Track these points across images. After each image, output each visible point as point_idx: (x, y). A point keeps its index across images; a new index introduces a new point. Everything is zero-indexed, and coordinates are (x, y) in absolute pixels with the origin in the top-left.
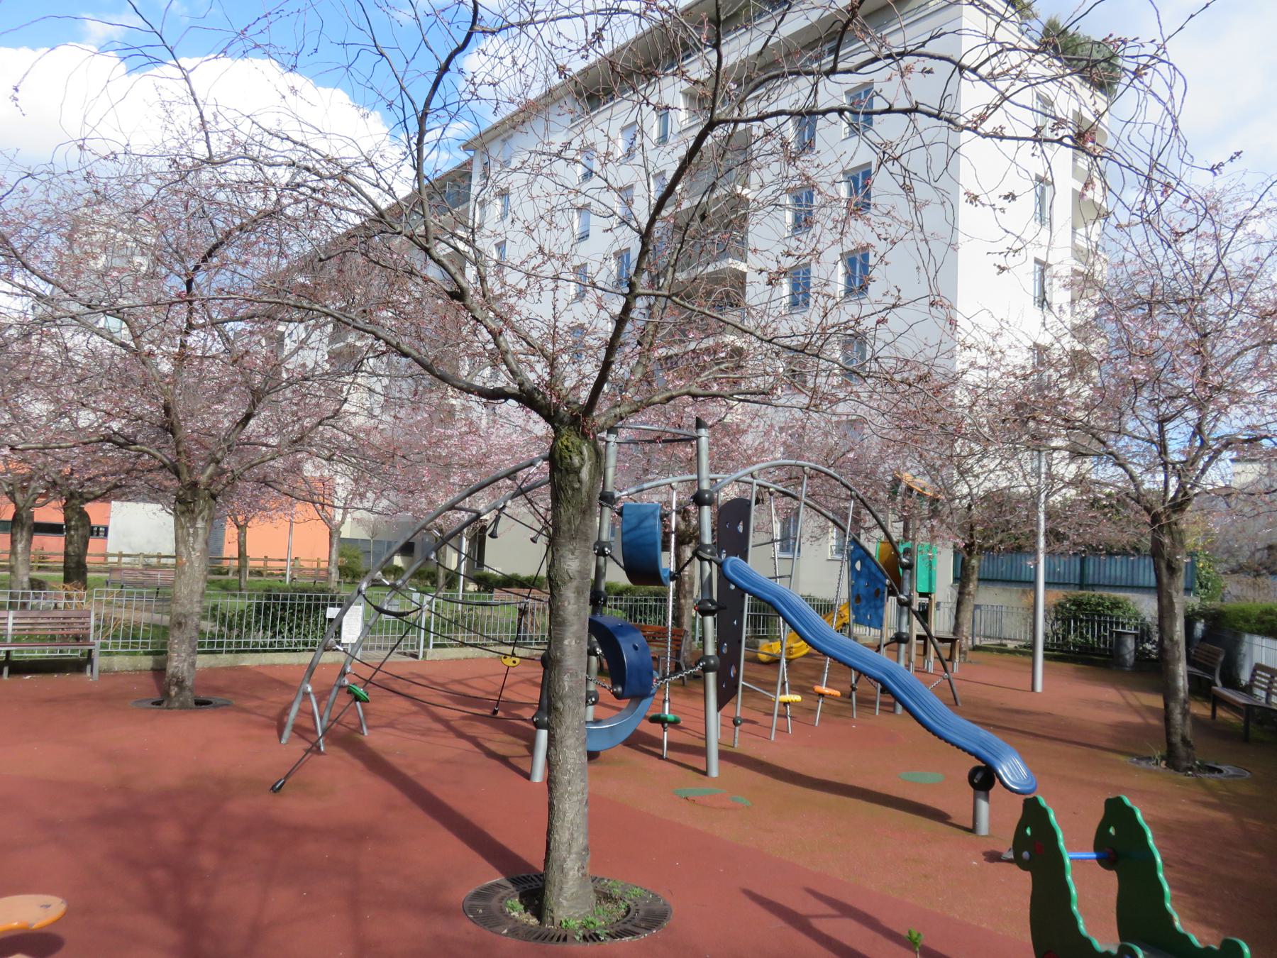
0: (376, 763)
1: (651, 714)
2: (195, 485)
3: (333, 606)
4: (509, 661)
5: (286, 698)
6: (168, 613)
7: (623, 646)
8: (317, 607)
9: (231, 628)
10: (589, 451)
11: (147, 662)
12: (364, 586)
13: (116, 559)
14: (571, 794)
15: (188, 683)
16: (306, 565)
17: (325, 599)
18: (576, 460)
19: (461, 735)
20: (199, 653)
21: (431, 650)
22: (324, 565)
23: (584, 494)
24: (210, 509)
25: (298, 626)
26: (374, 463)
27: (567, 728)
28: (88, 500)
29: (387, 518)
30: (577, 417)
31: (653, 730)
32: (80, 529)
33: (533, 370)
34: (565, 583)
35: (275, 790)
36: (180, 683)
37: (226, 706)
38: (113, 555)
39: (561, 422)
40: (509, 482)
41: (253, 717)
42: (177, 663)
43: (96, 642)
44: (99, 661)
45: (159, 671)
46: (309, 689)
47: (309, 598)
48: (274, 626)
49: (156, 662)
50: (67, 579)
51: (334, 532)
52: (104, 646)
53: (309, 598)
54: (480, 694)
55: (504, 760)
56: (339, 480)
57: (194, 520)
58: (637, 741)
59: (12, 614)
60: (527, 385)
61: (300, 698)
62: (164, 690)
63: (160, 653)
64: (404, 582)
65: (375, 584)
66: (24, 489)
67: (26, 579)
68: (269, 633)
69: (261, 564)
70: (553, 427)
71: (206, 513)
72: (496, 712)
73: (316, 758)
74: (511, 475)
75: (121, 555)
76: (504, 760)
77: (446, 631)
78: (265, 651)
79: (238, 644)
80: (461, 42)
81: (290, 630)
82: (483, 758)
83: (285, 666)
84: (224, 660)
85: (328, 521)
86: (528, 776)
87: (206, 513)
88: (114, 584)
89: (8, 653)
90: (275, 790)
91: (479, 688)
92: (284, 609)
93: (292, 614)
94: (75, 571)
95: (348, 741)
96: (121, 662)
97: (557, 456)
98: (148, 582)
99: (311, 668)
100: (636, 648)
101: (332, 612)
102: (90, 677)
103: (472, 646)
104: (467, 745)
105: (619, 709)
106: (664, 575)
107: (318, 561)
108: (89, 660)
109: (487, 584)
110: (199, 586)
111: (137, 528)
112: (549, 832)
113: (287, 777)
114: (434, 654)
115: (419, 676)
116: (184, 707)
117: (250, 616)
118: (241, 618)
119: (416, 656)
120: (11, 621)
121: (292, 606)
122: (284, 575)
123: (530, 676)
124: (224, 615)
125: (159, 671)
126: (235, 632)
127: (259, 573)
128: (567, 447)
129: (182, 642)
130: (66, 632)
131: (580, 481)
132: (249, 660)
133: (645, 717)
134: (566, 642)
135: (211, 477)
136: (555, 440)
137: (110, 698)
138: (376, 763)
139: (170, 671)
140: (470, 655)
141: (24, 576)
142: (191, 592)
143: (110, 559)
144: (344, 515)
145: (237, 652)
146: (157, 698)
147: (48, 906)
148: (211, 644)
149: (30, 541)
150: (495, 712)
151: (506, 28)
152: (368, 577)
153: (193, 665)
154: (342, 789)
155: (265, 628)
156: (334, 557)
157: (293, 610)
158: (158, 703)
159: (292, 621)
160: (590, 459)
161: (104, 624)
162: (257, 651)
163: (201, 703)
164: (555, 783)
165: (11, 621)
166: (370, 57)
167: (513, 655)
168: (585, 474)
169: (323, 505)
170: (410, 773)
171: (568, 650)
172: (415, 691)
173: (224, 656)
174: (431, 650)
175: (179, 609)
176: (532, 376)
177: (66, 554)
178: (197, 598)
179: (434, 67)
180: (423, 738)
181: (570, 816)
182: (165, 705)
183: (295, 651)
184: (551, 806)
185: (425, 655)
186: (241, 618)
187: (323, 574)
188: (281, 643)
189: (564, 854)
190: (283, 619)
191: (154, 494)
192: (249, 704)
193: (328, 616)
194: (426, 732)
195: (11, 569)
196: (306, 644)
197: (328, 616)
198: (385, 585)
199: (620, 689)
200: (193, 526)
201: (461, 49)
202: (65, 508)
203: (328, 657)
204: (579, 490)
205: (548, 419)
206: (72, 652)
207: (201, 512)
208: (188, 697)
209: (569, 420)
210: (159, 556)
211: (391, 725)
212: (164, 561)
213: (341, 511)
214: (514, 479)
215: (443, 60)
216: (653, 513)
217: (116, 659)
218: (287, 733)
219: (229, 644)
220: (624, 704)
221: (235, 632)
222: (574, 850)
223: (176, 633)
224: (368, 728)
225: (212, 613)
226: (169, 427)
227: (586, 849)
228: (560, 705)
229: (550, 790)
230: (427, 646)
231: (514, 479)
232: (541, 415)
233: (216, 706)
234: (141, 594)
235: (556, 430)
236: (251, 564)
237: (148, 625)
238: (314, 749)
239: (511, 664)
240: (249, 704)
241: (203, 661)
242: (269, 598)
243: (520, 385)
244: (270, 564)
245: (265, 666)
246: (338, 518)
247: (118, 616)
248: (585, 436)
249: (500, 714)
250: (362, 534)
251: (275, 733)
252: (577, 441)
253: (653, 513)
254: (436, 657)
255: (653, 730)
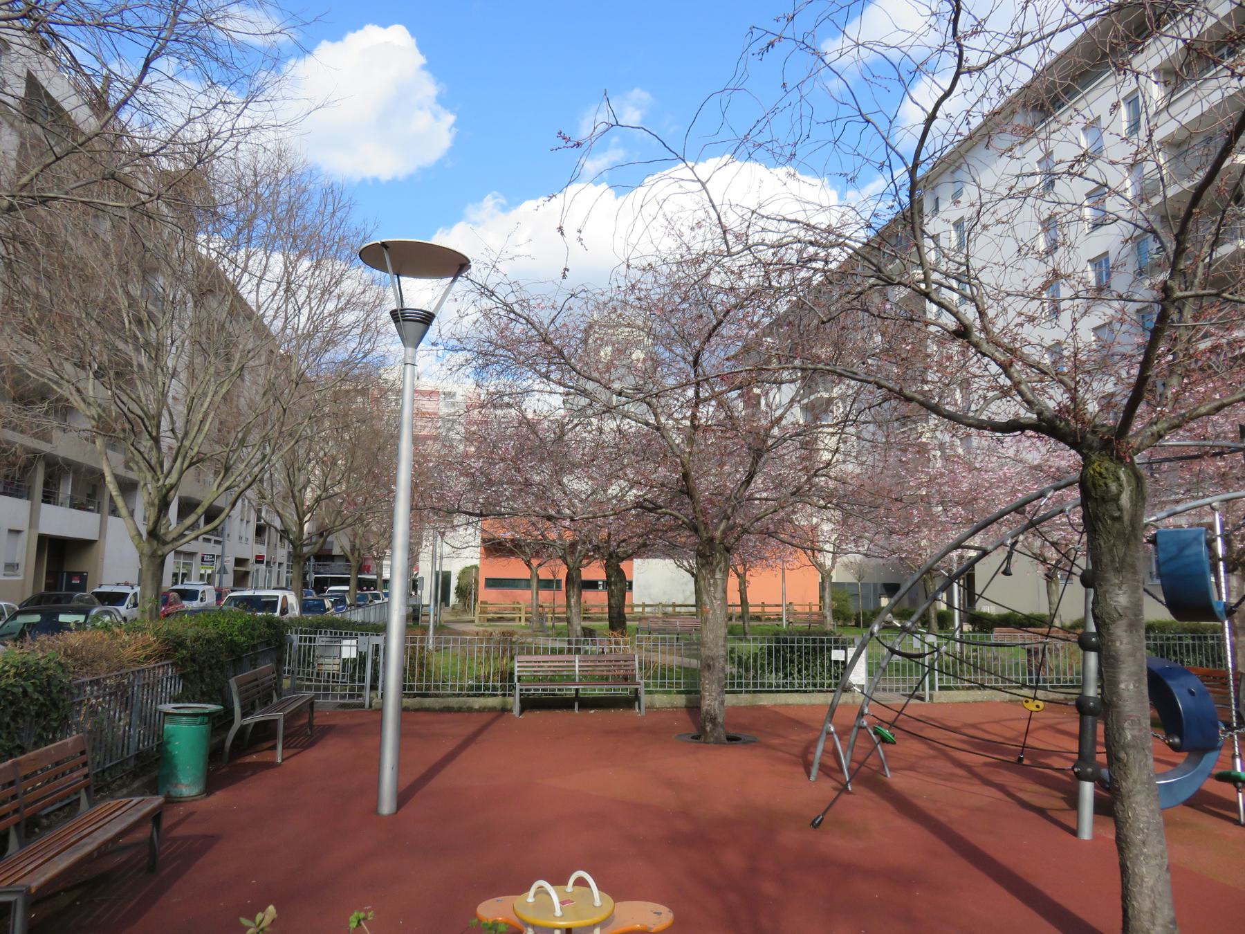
0: (903, 805)
1: (1216, 771)
2: (712, 539)
3: (837, 648)
4: (1031, 706)
5: (811, 736)
6: (697, 657)
7: (1175, 690)
8: (822, 649)
9: (747, 670)
10: (1128, 476)
11: (681, 700)
12: (876, 628)
13: (640, 609)
14: (1147, 857)
15: (720, 720)
16: (799, 609)
17: (829, 641)
18: (1113, 487)
19: (987, 782)
20: (727, 692)
21: (937, 692)
22: (815, 609)
23: (1126, 518)
24: (726, 561)
25: (807, 668)
26: (854, 505)
27: (1135, 782)
28: (623, 559)
29: (881, 561)
30: (1109, 441)
31: (1224, 790)
32: (619, 584)
33: (1051, 398)
34: (1114, 621)
35: (815, 825)
36: (713, 720)
37: (752, 743)
38: (638, 606)
39: (1090, 448)
40: (1019, 517)
41: (780, 754)
42: (710, 701)
43: (641, 681)
44: (645, 699)
45: (693, 708)
46: (832, 729)
47: (814, 641)
48: (785, 668)
49: (688, 700)
50: (612, 627)
51: (826, 576)
52: (647, 685)
53: (814, 641)
54: (1001, 740)
55: (1041, 812)
56: (826, 527)
57: (713, 572)
58: (1200, 802)
59: (577, 658)
60: (1047, 413)
61: (823, 737)
62: (699, 726)
63: (693, 692)
64: (913, 624)
65: (888, 626)
66: (572, 553)
67: (579, 628)
68: (781, 674)
69: (759, 609)
70: (1081, 454)
71: (722, 565)
72: (1022, 759)
73: (844, 796)
74: (1019, 508)
75: (644, 606)
76: (1041, 812)
77: (954, 671)
78: (778, 692)
79: (755, 685)
80: (947, 87)
81: (800, 671)
82: (1017, 809)
83: (798, 706)
84: (744, 699)
85: (820, 567)
86: (1075, 832)
87: (722, 565)
88: (643, 630)
89: (577, 690)
90: (815, 825)
91: (995, 732)
92: (792, 652)
93: (800, 656)
94: (617, 620)
95: (871, 780)
96: (660, 700)
97: (1089, 484)
98: (664, 625)
99: (832, 708)
100: (1192, 693)
101: (837, 655)
102: (638, 713)
103: (991, 688)
104: (999, 795)
105: (1174, 765)
106: (1219, 609)
107: (810, 605)
108: (636, 697)
109: (983, 623)
110: (723, 631)
111: (658, 581)
112: (1126, 897)
113: (824, 814)
114: (941, 697)
115: (932, 719)
116: (717, 741)
117: (763, 659)
118: (755, 661)
119: (922, 699)
120: (577, 664)
121: (799, 649)
122: (781, 620)
123: (1052, 722)
124: (740, 658)
125: (693, 708)
126: (752, 673)
127: (758, 618)
128: (1100, 474)
129: (711, 683)
130: (617, 673)
131: (1120, 509)
132: (766, 700)
133: (1210, 776)
134: (1122, 686)
135: (724, 532)
136: (1084, 467)
137: (656, 732)
138: (903, 805)
139: (704, 708)
140: (979, 699)
141: (578, 625)
142: (715, 639)
143: (636, 610)
144: (834, 560)
145: (755, 692)
146: (694, 732)
147: (659, 914)
148: (732, 684)
149: (579, 596)
150: (1020, 760)
151: (994, 61)
152: (879, 619)
153: (722, 703)
154: (876, 834)
155: (777, 670)
156: (828, 600)
157: (798, 652)
158: (696, 738)
159: (800, 663)
160: (1128, 481)
161: (644, 666)
162: (772, 692)
163: (732, 739)
164: (1126, 843)
165: (577, 664)
166: (856, 127)
167: (1035, 698)
168: (1125, 500)
169: (813, 550)
170: (942, 818)
171: (1125, 694)
172: (929, 733)
173: (744, 696)
174: (937, 692)
175: (708, 653)
176: (1052, 404)
177: (610, 606)
178: (721, 642)
179: (923, 117)
180: (949, 784)
181: (1149, 881)
182: (702, 739)
183: (805, 692)
184: (1124, 869)
185: (931, 697)
186: (755, 661)
187: (815, 618)
188: (792, 685)
189: (1147, 925)
190: (792, 661)
191: (671, 551)
192: (776, 741)
193: (833, 658)
194: (950, 777)
195: (568, 620)
196: (815, 685)
197: (833, 658)
198: (896, 627)
199: (1177, 740)
200: (713, 577)
201: (947, 94)
202: (606, 567)
203: (845, 698)
204: (1119, 519)
205: (1073, 445)
206: (622, 691)
207: (718, 564)
208: (721, 733)
209: (1097, 445)
210: (674, 606)
211: (911, 768)
212: (678, 609)
213: (830, 555)
214: (1023, 513)
215: (930, 111)
216: (1196, 539)
217: (656, 696)
218: (814, 771)
219: (747, 685)
220: (1180, 758)
221: (752, 673)
222: (1159, 921)
223: (707, 674)
224: (891, 770)
225: (731, 656)
226: (686, 489)
227: (1173, 922)
228: (1123, 755)
229: (1121, 850)
230: (932, 687)
231: (1023, 513)
232: (1067, 443)
233: (746, 743)
234: (664, 639)
235: (1085, 458)
236: (751, 609)
237: (679, 667)
238: (844, 789)
239: (1034, 709)
240: (776, 741)
241: (730, 700)
242: (778, 641)
243: (1039, 414)
244: (767, 609)
245: (781, 706)
246: (828, 563)
247: (655, 659)
248: (1120, 460)
249: (1025, 762)
250: (848, 577)
251: (802, 770)
252: (1112, 467)
253: (1196, 539)
254: (943, 700)
255: (1224, 790)
